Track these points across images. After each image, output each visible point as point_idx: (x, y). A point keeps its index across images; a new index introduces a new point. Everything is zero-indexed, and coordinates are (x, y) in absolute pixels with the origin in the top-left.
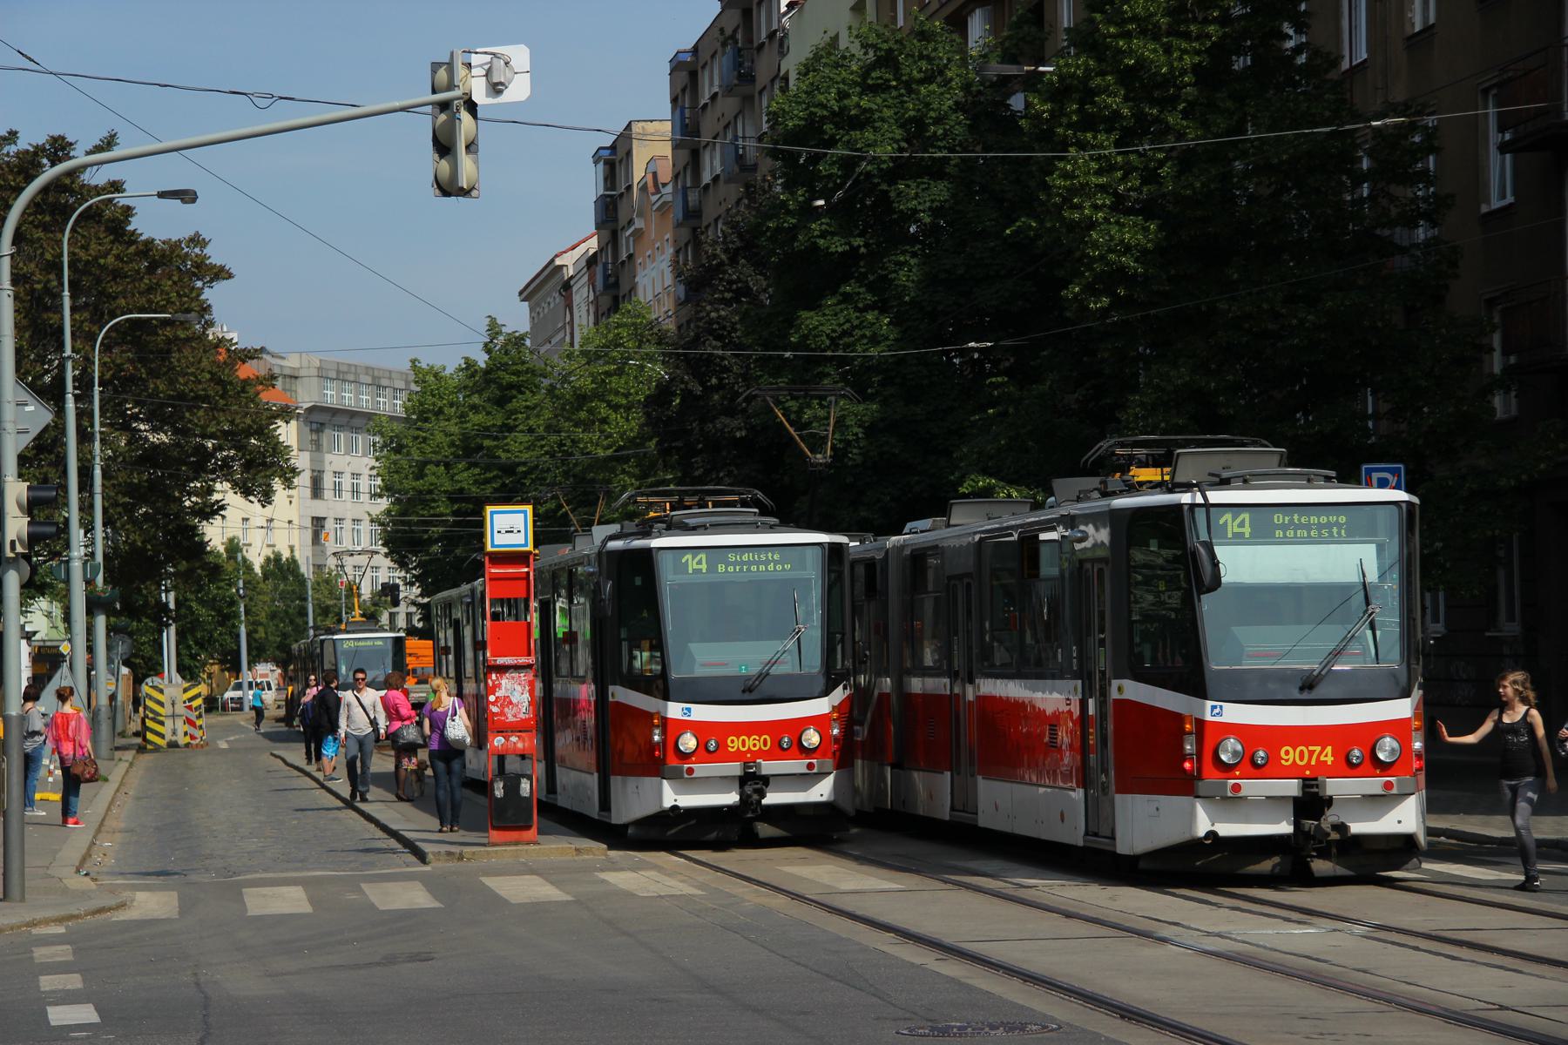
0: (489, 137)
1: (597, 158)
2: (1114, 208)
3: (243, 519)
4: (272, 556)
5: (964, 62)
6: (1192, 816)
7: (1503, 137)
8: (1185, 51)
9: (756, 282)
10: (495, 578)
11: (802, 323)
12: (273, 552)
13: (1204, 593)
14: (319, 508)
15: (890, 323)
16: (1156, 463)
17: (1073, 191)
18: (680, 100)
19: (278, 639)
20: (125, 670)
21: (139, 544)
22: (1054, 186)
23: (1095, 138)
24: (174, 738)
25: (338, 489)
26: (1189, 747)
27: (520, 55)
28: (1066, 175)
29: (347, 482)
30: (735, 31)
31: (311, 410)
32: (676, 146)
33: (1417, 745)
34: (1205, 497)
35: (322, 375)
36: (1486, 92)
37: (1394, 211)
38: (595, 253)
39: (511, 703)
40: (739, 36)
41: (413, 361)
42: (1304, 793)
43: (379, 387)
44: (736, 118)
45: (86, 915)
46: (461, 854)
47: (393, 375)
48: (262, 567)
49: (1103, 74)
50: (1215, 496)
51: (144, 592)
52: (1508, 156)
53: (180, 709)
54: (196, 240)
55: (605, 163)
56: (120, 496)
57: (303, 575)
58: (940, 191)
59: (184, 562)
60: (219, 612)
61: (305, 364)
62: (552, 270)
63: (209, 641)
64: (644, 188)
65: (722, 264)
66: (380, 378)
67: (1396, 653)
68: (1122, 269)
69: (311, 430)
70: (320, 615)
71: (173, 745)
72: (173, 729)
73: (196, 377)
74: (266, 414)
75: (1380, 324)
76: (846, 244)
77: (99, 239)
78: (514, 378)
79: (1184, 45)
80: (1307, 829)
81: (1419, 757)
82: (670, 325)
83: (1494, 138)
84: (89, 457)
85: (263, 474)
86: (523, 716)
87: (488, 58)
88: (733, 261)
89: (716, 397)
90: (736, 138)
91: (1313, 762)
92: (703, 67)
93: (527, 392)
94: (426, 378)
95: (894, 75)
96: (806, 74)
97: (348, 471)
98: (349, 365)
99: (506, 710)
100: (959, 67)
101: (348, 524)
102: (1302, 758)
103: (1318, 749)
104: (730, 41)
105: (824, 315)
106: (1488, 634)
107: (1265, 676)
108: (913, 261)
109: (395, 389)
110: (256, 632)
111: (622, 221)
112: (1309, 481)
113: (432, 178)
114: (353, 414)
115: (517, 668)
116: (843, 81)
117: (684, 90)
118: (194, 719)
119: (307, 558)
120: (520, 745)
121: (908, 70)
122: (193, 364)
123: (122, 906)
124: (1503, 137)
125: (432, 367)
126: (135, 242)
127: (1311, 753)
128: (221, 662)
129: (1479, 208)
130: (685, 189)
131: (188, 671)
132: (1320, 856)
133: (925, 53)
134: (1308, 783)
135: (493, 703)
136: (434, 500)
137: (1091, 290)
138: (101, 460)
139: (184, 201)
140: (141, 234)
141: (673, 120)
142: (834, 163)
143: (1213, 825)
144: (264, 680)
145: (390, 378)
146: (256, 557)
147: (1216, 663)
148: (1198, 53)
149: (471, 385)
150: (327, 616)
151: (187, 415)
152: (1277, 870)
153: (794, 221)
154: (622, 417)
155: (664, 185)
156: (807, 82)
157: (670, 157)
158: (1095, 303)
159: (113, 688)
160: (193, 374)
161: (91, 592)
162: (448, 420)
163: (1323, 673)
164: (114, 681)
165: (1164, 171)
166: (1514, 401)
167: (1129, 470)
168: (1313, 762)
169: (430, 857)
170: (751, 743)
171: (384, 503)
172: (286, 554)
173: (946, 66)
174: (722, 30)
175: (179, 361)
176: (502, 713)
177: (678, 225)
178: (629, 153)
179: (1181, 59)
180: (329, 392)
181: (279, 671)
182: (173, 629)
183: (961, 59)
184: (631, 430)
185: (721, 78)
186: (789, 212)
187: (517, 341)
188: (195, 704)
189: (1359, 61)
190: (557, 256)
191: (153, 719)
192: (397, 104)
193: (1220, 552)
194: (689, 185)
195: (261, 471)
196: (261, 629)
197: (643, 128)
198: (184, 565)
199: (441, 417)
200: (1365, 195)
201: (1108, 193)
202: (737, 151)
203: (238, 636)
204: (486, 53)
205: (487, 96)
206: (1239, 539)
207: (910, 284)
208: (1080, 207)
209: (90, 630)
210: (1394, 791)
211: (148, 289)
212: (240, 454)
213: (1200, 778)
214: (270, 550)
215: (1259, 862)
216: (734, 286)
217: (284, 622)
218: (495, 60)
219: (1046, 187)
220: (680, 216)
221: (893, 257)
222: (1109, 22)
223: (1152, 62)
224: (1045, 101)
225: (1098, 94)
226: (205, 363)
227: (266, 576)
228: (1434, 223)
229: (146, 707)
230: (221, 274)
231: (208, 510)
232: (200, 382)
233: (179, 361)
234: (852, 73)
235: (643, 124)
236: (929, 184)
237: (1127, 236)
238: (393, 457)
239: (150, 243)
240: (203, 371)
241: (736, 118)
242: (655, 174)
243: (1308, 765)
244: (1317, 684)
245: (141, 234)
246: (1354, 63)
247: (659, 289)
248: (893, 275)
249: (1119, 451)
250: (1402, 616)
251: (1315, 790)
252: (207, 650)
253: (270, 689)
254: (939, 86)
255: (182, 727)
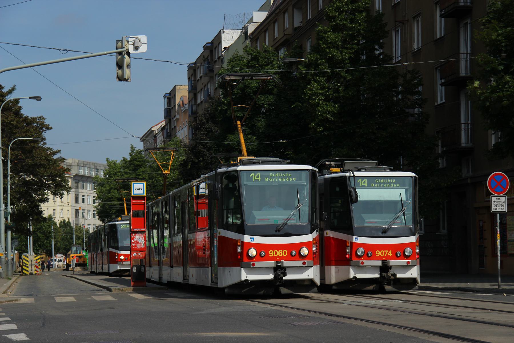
0: (134, 63)
1: (165, 97)
2: (324, 100)
3: (54, 209)
4: (62, 221)
5: (278, 60)
6: (349, 272)
7: (442, 82)
8: (346, 53)
9: (214, 128)
10: (134, 204)
11: (229, 138)
12: (63, 220)
13: (353, 203)
14: (77, 206)
15: (256, 139)
16: (337, 166)
17: (312, 95)
18: (191, 78)
19: (64, 247)
20: (16, 252)
21: (22, 210)
22: (307, 93)
23: (319, 79)
24: (31, 272)
25: (83, 201)
26: (348, 251)
27: (144, 38)
28: (310, 90)
29: (86, 198)
30: (208, 57)
31: (75, 176)
32: (189, 93)
33: (417, 251)
34: (353, 174)
35: (79, 165)
36: (436, 68)
37: (409, 103)
38: (164, 126)
39: (138, 243)
40: (209, 58)
41: (107, 159)
42: (383, 265)
43: (96, 168)
44: (208, 83)
45: (5, 302)
46: (122, 289)
47: (101, 165)
48: (59, 224)
49: (322, 59)
50: (357, 174)
51: (23, 225)
52: (443, 87)
53: (34, 263)
54: (41, 117)
55: (167, 99)
56: (16, 195)
57: (72, 227)
58: (271, 99)
59: (36, 216)
60: (46, 236)
61: (73, 162)
62: (151, 132)
63: (43, 245)
64: (179, 106)
65: (204, 123)
66: (96, 166)
67: (411, 223)
68: (327, 119)
69: (75, 182)
70: (77, 239)
71: (31, 274)
72: (31, 269)
73: (40, 158)
74: (62, 170)
75: (405, 137)
76: (242, 114)
77: (11, 116)
78: (139, 163)
79: (346, 51)
80: (384, 276)
81: (418, 254)
82: (186, 141)
83: (439, 82)
84: (7, 183)
85: (61, 189)
86: (142, 247)
87: (134, 39)
88: (207, 122)
89: (202, 164)
90: (208, 89)
91: (386, 256)
92: (198, 68)
93: (143, 167)
94: (112, 165)
95: (257, 63)
96: (230, 63)
97: (87, 209)
98: (87, 162)
99: (137, 245)
100: (277, 61)
101: (86, 211)
102: (382, 254)
103: (387, 251)
104: (206, 60)
105: (235, 136)
106: (437, 233)
107: (372, 229)
108: (263, 120)
109: (101, 170)
110: (57, 244)
111: (173, 116)
112: (385, 170)
113: (116, 76)
114: (88, 177)
115: (141, 232)
116: (242, 65)
117: (192, 75)
118: (38, 266)
119: (74, 221)
120: (141, 256)
121: (261, 62)
122: (39, 154)
123: (17, 300)
124: (442, 82)
125: (113, 161)
126: (22, 117)
127: (385, 253)
128: (46, 254)
129: (435, 104)
130: (192, 105)
131: (36, 252)
132: (387, 285)
133: (266, 57)
134: (384, 262)
135: (133, 243)
136: (113, 201)
137: (318, 125)
138: (10, 183)
139: (37, 100)
140: (24, 115)
141: (188, 85)
142: (238, 89)
143: (355, 274)
144: (59, 259)
145: (100, 166)
146: (58, 221)
147: (356, 225)
148: (350, 53)
149: (125, 166)
150: (79, 239)
151: (37, 170)
152: (375, 288)
153: (226, 107)
154: (172, 172)
155: (186, 104)
156: (231, 65)
157: (187, 96)
158: (319, 129)
159: (12, 256)
160: (39, 157)
161: (6, 224)
162: (118, 176)
163: (389, 228)
164: (13, 254)
165: (340, 89)
166: (445, 162)
167: (330, 169)
168: (386, 256)
169: (113, 290)
170: (279, 253)
171: (97, 202)
172: (67, 220)
173: (273, 61)
174: (204, 56)
175: (35, 153)
176: (136, 246)
177: (190, 116)
178: (175, 95)
179: (345, 55)
180: (81, 170)
181: (64, 257)
182: (31, 237)
183: (277, 59)
184: (175, 177)
185: (203, 71)
186: (225, 105)
187: (140, 152)
188: (38, 261)
189: (398, 60)
190: (152, 127)
191: (25, 266)
192: (106, 52)
193: (358, 191)
194: (193, 104)
195: (60, 188)
196: (59, 243)
197: (179, 87)
198: (35, 217)
199: (116, 176)
200: (400, 98)
201: (323, 95)
202: (208, 93)
203: (51, 245)
204: (133, 37)
205: (133, 51)
206: (363, 187)
207: (262, 127)
208: (315, 100)
209: (6, 238)
210: (410, 264)
211: (26, 131)
212: (54, 182)
213: (351, 260)
214: (62, 219)
215: (369, 286)
216: (208, 130)
217: (66, 241)
218: (136, 40)
219: (304, 94)
220: (190, 113)
221: (257, 119)
222: (323, 43)
223: (336, 56)
224: (304, 68)
225: (320, 65)
226: (43, 154)
227: (60, 226)
228: (421, 107)
229: (23, 262)
230: (48, 128)
231: (43, 200)
232: (42, 160)
233: (35, 153)
234: (244, 62)
235: (179, 86)
236: (268, 96)
237: (329, 108)
238: (101, 188)
239: (27, 118)
240: (42, 156)
241: (208, 83)
242: (183, 101)
243: (384, 256)
244: (387, 231)
245: (24, 115)
246: (397, 61)
247: (184, 136)
248: (257, 124)
249: (327, 163)
250: (413, 212)
251: (386, 264)
252: (42, 248)
253: (61, 261)
254: (271, 66)
255: (34, 268)
